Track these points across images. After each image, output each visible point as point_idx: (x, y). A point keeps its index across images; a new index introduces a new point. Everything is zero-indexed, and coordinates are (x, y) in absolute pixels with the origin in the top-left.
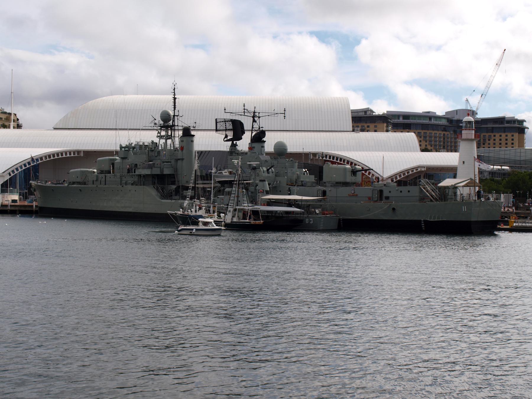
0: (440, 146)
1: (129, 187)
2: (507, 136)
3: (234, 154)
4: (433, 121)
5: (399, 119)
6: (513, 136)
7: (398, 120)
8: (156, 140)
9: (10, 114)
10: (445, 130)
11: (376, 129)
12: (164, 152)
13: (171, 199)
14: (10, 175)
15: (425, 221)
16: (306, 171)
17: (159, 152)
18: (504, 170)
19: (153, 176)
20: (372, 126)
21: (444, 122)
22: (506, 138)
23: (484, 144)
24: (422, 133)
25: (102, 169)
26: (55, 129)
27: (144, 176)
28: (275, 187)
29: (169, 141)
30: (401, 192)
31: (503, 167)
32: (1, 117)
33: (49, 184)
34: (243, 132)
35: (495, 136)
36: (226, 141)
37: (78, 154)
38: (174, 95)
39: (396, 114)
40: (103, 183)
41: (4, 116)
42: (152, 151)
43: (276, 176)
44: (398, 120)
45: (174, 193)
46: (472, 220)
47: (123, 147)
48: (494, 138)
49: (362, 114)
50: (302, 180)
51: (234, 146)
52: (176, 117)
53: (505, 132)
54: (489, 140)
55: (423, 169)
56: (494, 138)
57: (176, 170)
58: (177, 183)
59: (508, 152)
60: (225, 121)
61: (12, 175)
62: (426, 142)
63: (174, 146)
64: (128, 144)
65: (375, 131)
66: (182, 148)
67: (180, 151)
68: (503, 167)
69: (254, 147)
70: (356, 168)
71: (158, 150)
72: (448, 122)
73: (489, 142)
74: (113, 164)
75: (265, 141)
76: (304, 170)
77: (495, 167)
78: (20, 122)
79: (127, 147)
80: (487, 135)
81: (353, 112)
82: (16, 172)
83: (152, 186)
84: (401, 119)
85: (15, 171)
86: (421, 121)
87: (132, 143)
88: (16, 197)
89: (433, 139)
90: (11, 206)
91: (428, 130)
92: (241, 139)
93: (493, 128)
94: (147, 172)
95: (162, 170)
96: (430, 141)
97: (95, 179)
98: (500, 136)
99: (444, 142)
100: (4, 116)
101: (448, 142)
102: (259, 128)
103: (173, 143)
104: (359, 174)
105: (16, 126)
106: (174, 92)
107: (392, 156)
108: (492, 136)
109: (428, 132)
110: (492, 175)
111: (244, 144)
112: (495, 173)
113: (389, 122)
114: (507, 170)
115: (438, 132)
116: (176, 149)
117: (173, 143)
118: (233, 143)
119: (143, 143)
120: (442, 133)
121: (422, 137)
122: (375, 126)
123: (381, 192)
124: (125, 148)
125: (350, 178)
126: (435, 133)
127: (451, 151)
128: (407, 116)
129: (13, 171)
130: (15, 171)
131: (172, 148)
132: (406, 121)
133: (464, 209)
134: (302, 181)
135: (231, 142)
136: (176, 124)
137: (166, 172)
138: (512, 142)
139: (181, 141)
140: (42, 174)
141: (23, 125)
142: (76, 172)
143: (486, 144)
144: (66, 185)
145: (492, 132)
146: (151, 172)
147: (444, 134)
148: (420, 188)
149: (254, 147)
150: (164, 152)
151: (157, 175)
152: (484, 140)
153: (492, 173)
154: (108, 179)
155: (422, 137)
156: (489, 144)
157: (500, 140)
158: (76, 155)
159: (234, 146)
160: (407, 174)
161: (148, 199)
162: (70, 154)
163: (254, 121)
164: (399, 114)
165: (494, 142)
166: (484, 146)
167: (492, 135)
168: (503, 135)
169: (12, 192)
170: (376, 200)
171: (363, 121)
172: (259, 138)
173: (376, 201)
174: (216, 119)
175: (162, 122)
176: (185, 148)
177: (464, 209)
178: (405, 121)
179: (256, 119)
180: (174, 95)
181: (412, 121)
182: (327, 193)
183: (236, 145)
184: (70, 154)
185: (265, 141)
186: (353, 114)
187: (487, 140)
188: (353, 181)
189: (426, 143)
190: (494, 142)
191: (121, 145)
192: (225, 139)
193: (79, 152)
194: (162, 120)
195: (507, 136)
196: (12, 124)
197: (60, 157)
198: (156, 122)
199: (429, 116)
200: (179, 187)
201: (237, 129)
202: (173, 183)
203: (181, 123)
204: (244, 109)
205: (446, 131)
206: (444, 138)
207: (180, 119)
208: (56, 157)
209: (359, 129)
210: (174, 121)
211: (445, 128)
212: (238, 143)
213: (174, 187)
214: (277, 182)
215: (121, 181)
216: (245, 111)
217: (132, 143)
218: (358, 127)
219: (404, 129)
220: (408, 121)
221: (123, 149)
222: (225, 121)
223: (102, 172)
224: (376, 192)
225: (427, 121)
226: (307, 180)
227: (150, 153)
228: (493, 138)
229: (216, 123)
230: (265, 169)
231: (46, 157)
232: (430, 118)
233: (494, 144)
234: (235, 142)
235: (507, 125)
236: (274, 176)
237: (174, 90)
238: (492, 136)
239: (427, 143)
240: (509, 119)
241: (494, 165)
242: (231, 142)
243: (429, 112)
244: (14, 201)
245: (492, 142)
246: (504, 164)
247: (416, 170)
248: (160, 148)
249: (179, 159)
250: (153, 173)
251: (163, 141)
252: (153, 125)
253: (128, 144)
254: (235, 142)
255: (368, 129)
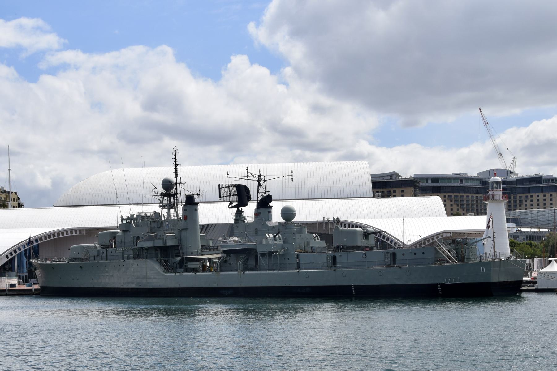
0: (473, 209)
1: (132, 261)
2: (545, 196)
3: (240, 222)
4: (465, 184)
5: (427, 182)
6: (551, 195)
7: (427, 184)
8: (159, 210)
9: (9, 192)
10: (478, 192)
11: (403, 193)
12: (167, 223)
13: (175, 272)
14: (7, 257)
15: (442, 285)
16: (317, 237)
17: (162, 223)
18: (542, 232)
19: (156, 248)
20: (398, 190)
21: (477, 184)
22: (545, 198)
23: (520, 206)
24: (453, 196)
25: (104, 244)
26: (55, 206)
27: (146, 249)
28: (283, 255)
29: (172, 211)
30: (415, 254)
31: (541, 230)
32: (1, 196)
33: (48, 262)
34: (249, 198)
35: (532, 196)
36: (231, 208)
37: (80, 232)
38: (176, 161)
39: (424, 176)
40: (105, 258)
41: (3, 196)
42: (155, 222)
43: (284, 242)
44: (427, 184)
45: (178, 266)
46: (492, 281)
47: (125, 219)
48: (531, 199)
49: (387, 179)
50: (311, 246)
51: (239, 213)
52: (178, 185)
53: (542, 192)
54: (526, 201)
55: (448, 235)
56: (531, 199)
57: (180, 241)
58: (181, 254)
59: (547, 213)
60: (229, 187)
61: (10, 257)
62: (458, 205)
63: (177, 216)
64: (129, 216)
65: (402, 196)
66: (185, 217)
67: (183, 220)
68: (541, 230)
69: (260, 213)
70: (367, 231)
71: (160, 221)
72: (480, 183)
73: (526, 203)
74: (115, 238)
75: (272, 206)
76: (315, 235)
77: (533, 230)
78: (21, 201)
79: (128, 218)
80: (523, 195)
81: (373, 176)
82: (14, 254)
83: (155, 259)
84: (430, 182)
85: (13, 253)
86: (451, 184)
87: (134, 215)
88: (15, 281)
89: (465, 202)
90: (9, 290)
91: (459, 193)
92: (247, 205)
93: (529, 188)
94: (149, 244)
95: (165, 242)
96: (462, 205)
97: (96, 254)
98: (538, 196)
99: (477, 206)
100: (3, 196)
101: (481, 205)
102: (265, 193)
103: (177, 212)
104: (372, 237)
105: (17, 205)
106: (175, 158)
107: (415, 221)
108: (529, 196)
109: (459, 195)
110: (530, 238)
111: (249, 211)
112: (533, 236)
113: (417, 186)
114: (545, 232)
115: (470, 195)
116: (179, 219)
117: (177, 212)
118: (238, 209)
119: (146, 214)
120: (475, 195)
121: (453, 201)
122: (402, 191)
123: (394, 255)
124: (126, 220)
125: (361, 242)
126: (461, 196)
127: (482, 215)
128: (436, 179)
129: (11, 254)
130: (13, 253)
131: (176, 218)
132: (436, 184)
133: (483, 269)
134: (312, 247)
135: (236, 209)
136: (179, 192)
137: (170, 243)
138: (551, 202)
139: (184, 210)
140: (42, 253)
141: (24, 204)
142: (76, 247)
143: (523, 206)
144: (67, 262)
145: (529, 193)
146: (154, 244)
147: (477, 197)
148: (436, 249)
149: (260, 213)
150: (167, 223)
151: (160, 248)
152: (521, 201)
153: (530, 236)
154: (109, 252)
155: (453, 201)
156: (526, 205)
157: (538, 200)
158: (78, 234)
159: (239, 213)
160: (431, 241)
161: (153, 274)
162: (72, 233)
163: (259, 185)
164: (427, 176)
165: (532, 203)
166: (520, 208)
167: (529, 195)
168: (541, 195)
169: (10, 276)
170: (389, 263)
171: (386, 186)
172: (265, 203)
173: (389, 265)
174: (219, 185)
175: (163, 191)
176: (188, 217)
177: (483, 269)
178: (434, 184)
179: (261, 183)
180: (176, 161)
181: (441, 184)
182: (338, 260)
183: (242, 211)
184: (72, 233)
185: (272, 206)
186: (374, 179)
187: (524, 201)
188: (366, 245)
189: (458, 207)
190: (532, 203)
191: (122, 217)
192: (231, 206)
193: (80, 230)
194: (164, 188)
195: (545, 196)
196: (11, 203)
197: (61, 236)
198: (156, 190)
199: (461, 178)
200: (182, 259)
201: (242, 195)
202: (178, 255)
203: (183, 191)
204: (248, 173)
205: (479, 193)
206: (477, 201)
207: (183, 186)
208: (57, 237)
209: (380, 194)
210: (176, 189)
211: (477, 191)
212: (244, 209)
213: (178, 259)
214: (284, 249)
215: (123, 255)
216: (249, 174)
217: (134, 215)
218: (378, 192)
219: (433, 192)
220: (438, 184)
221: (125, 222)
222: (229, 187)
223: (104, 247)
224: (389, 255)
225: (457, 184)
226: (317, 246)
227: (153, 224)
228: (530, 198)
229: (220, 188)
230: (271, 236)
231: (45, 237)
232: (461, 180)
233: (532, 205)
234: (240, 209)
235: (545, 185)
236: (281, 243)
237: (175, 156)
238: (529, 196)
239: (459, 207)
240: (546, 178)
241: (531, 228)
242: (236, 209)
243: (459, 174)
244: (12, 285)
245: (529, 203)
246: (543, 225)
247: (442, 236)
248: (163, 219)
249: (183, 229)
250: (156, 245)
251: (165, 211)
252: (154, 194)
253: (129, 216)
254: (240, 209)
255: (394, 194)
